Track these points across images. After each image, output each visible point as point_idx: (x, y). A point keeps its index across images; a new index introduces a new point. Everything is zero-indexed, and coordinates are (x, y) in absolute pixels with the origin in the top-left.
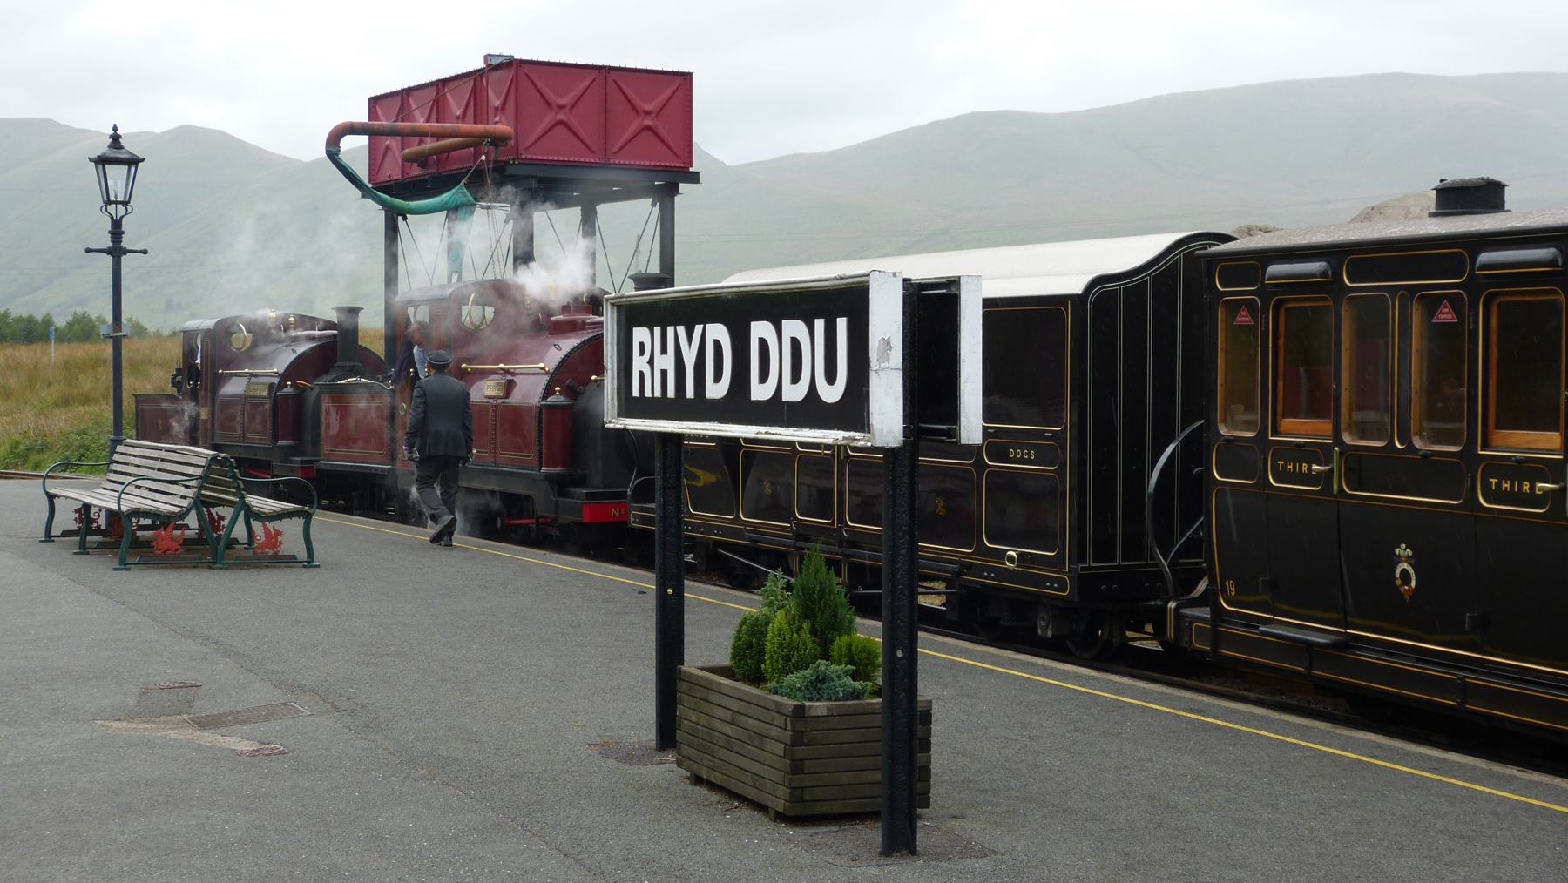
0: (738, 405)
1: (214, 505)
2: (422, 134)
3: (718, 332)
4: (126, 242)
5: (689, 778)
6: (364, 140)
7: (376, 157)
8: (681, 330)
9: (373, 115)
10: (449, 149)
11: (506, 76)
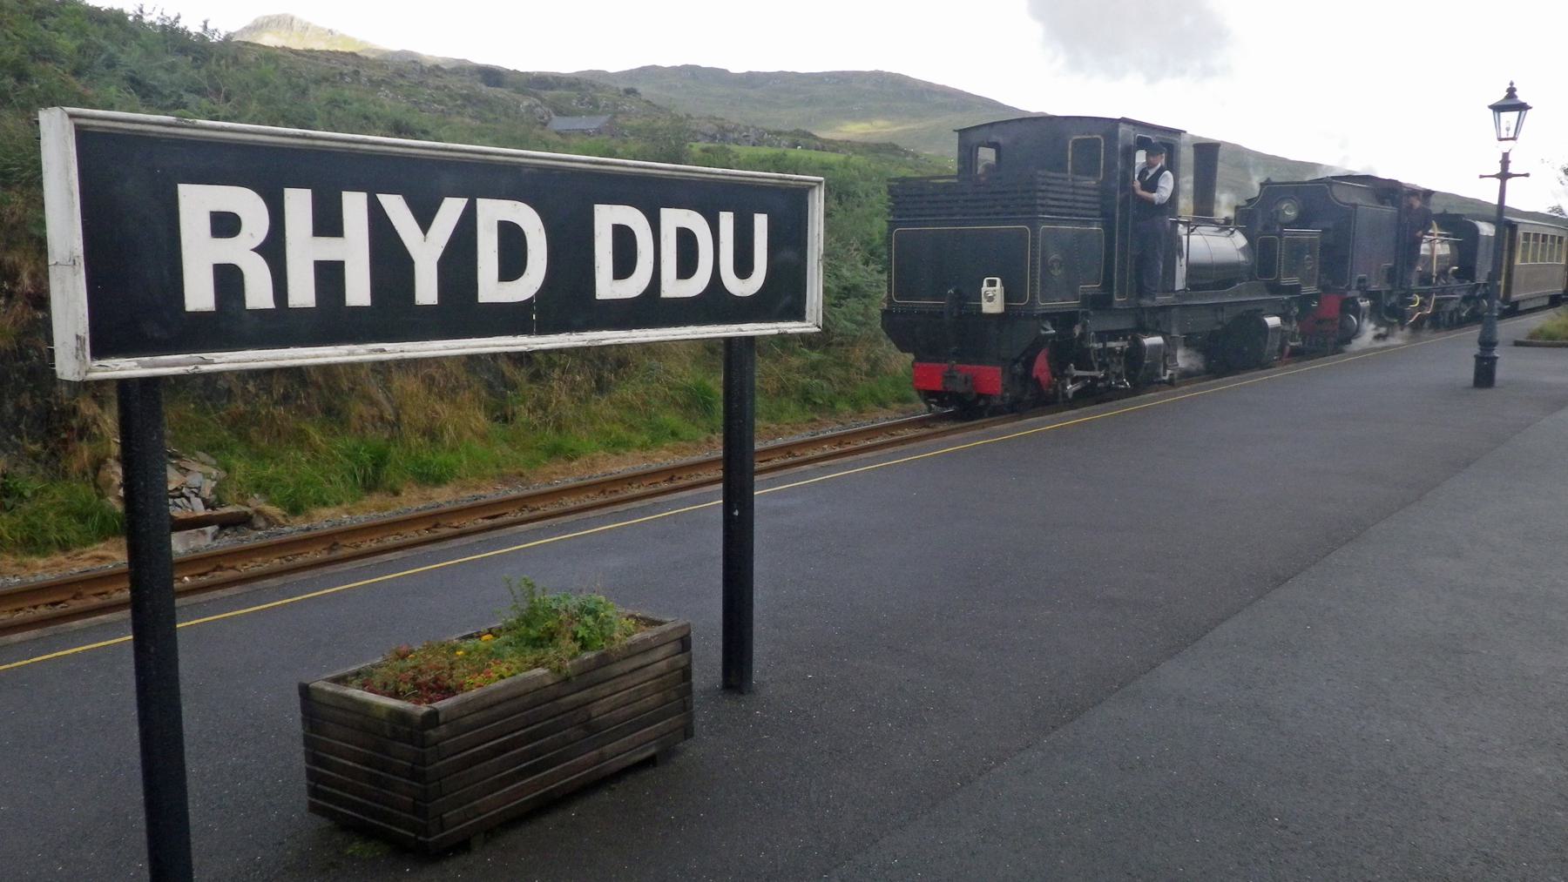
4: (1512, 169)
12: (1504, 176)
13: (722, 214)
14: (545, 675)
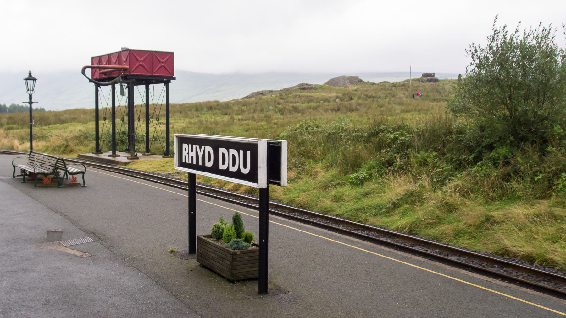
0: (215, 169)
1: (57, 169)
2: (105, 68)
3: (209, 149)
4: (33, 101)
5: (200, 265)
6: (90, 69)
7: (93, 75)
8: (198, 146)
9: (92, 63)
10: (111, 72)
11: (127, 53)
12: (31, 103)
13: (247, 152)
14: (197, 190)
